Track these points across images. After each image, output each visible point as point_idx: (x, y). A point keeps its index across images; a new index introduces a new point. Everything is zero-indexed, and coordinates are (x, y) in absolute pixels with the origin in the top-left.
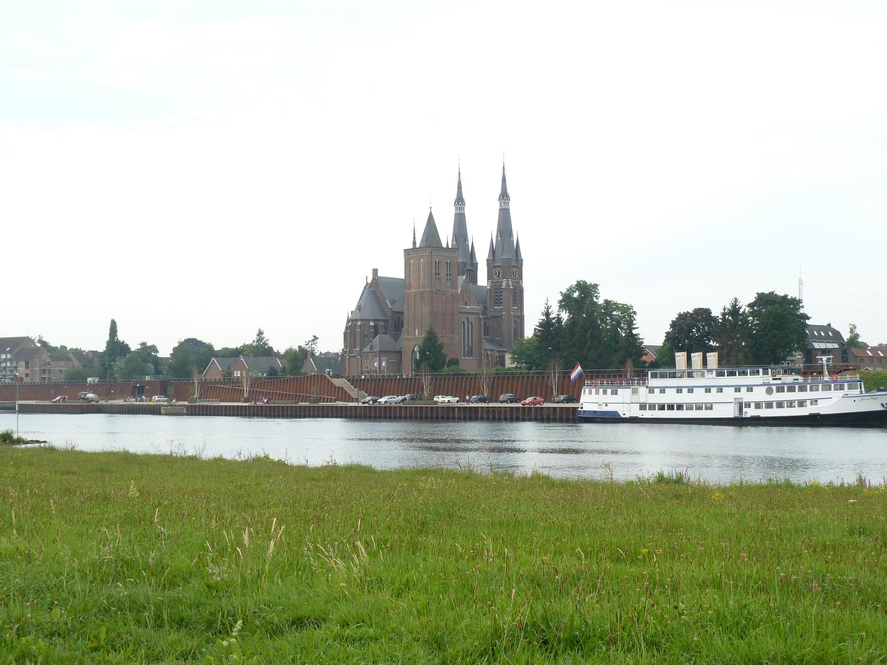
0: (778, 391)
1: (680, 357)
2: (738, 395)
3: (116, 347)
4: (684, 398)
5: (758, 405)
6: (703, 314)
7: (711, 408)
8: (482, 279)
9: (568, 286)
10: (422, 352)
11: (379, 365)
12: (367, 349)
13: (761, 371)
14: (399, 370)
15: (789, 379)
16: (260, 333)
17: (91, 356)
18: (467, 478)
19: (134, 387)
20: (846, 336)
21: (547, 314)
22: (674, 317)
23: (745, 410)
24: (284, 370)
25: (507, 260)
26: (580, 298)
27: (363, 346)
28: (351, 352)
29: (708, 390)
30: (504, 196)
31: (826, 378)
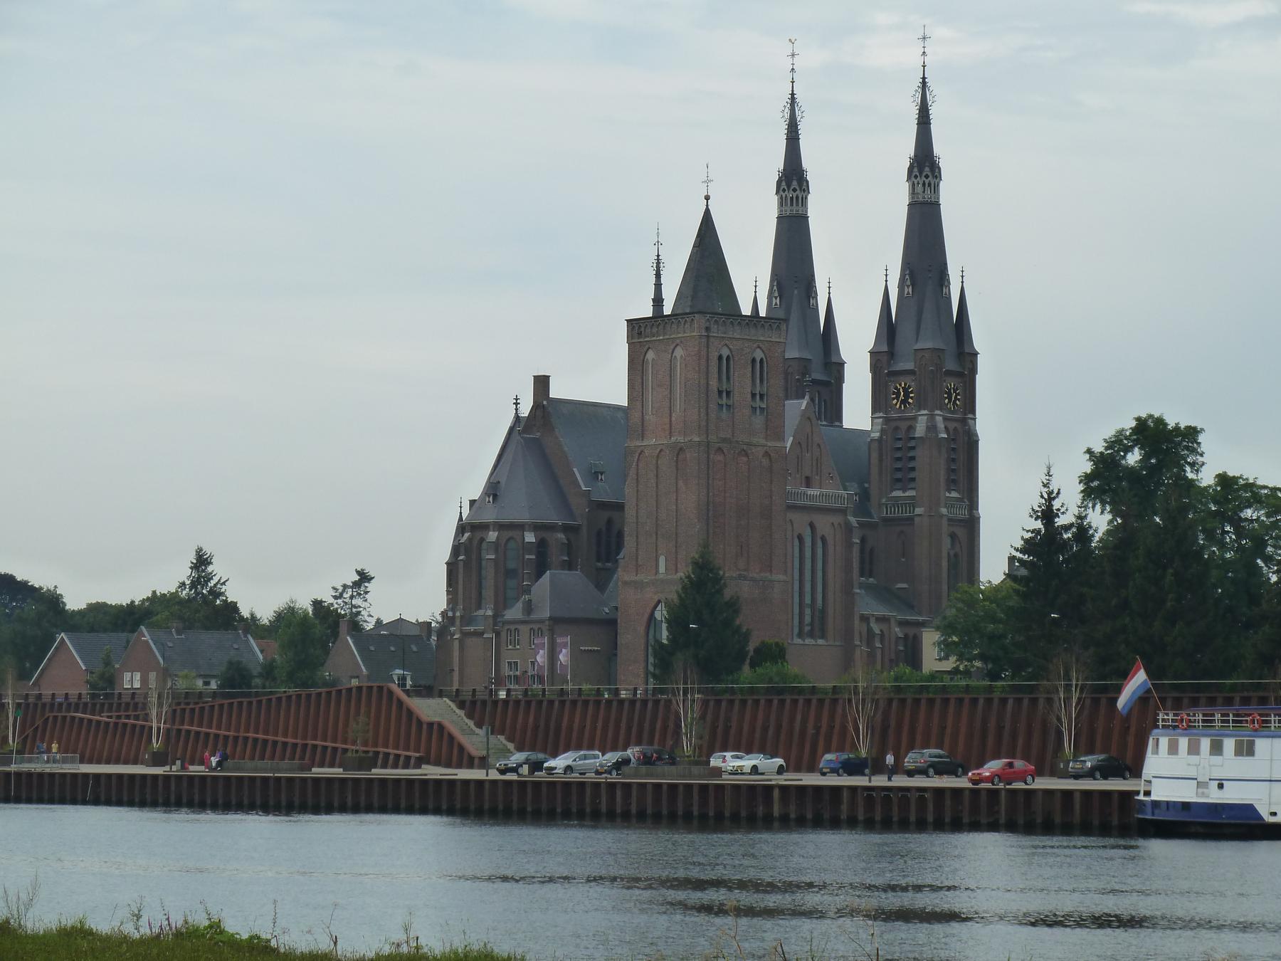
8: (857, 409)
9: (1110, 433)
10: (677, 622)
11: (549, 659)
14: (609, 676)
16: (202, 561)
21: (1048, 515)
24: (269, 671)
25: (932, 343)
27: (502, 603)
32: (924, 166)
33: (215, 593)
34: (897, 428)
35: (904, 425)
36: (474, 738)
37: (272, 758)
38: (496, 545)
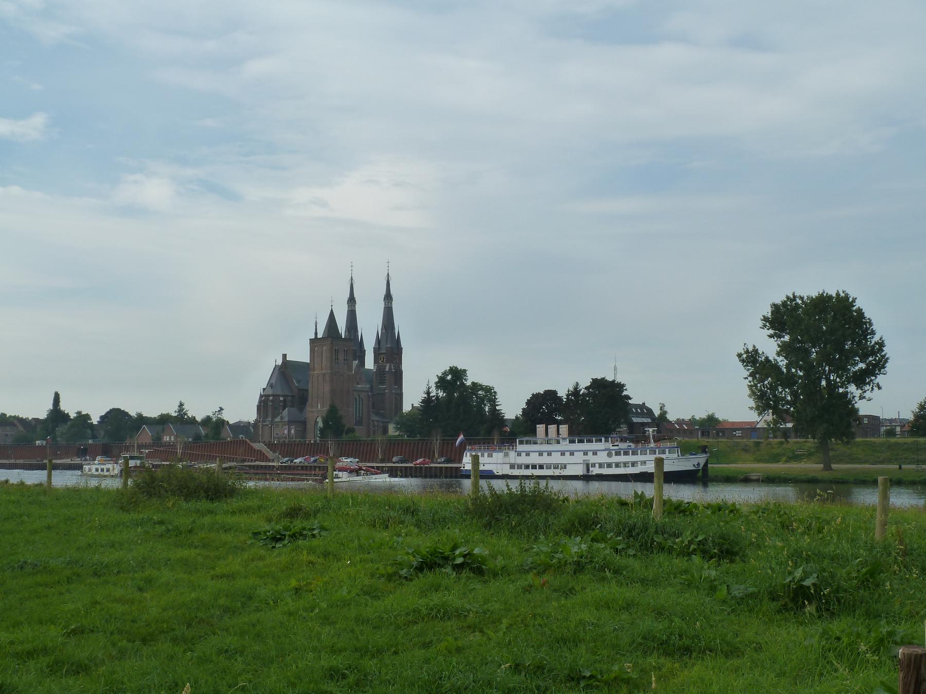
0: (616, 455)
1: (540, 428)
2: (586, 458)
3: (57, 415)
4: (545, 459)
5: (601, 466)
6: (551, 395)
7: (565, 468)
8: (369, 363)
9: (443, 371)
10: (325, 421)
11: (285, 432)
12: (278, 419)
13: (603, 439)
14: (304, 436)
15: (623, 446)
16: (181, 405)
17: (33, 423)
18: (732, 511)
19: (79, 449)
20: (657, 413)
21: (428, 393)
22: (529, 397)
23: (591, 469)
24: (207, 436)
25: (390, 348)
26: (453, 380)
27: (274, 417)
28: (264, 421)
29: (563, 454)
30: (388, 297)
31: (652, 445)
32: (388, 297)
33: (185, 414)
36: (270, 454)
38: (272, 401)
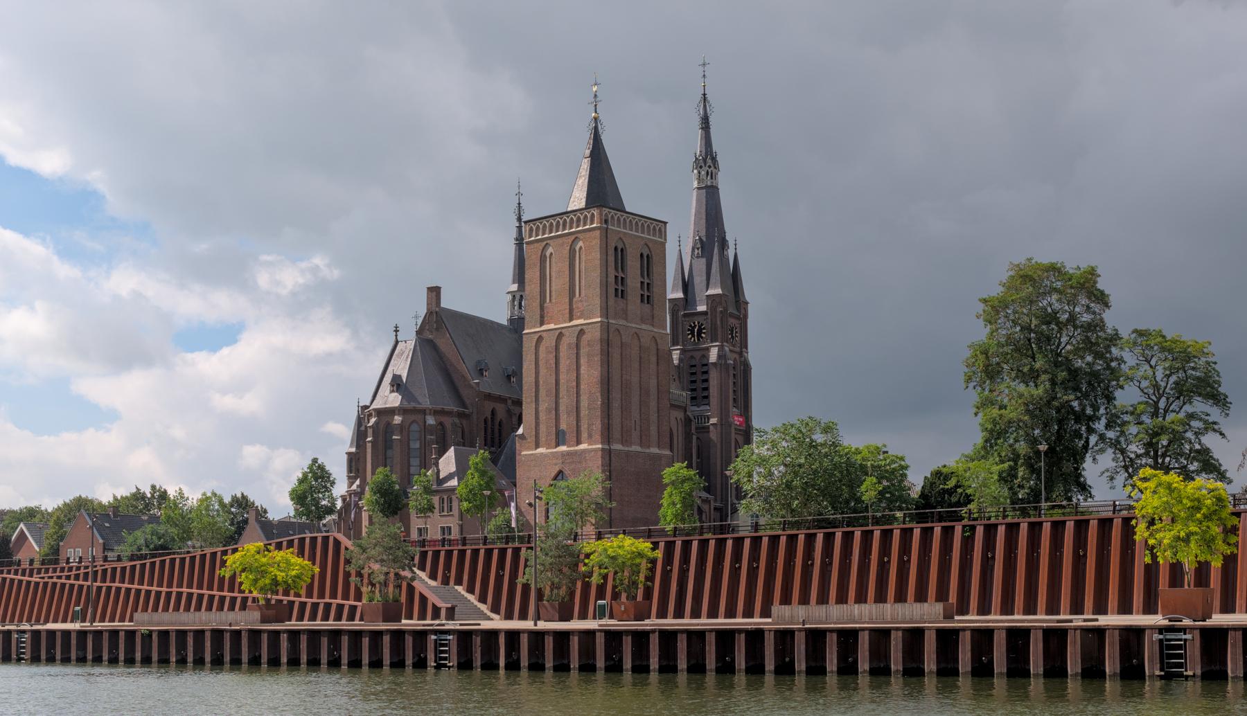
34: (692, 357)
35: (698, 355)
37: (804, 601)
38: (401, 426)
